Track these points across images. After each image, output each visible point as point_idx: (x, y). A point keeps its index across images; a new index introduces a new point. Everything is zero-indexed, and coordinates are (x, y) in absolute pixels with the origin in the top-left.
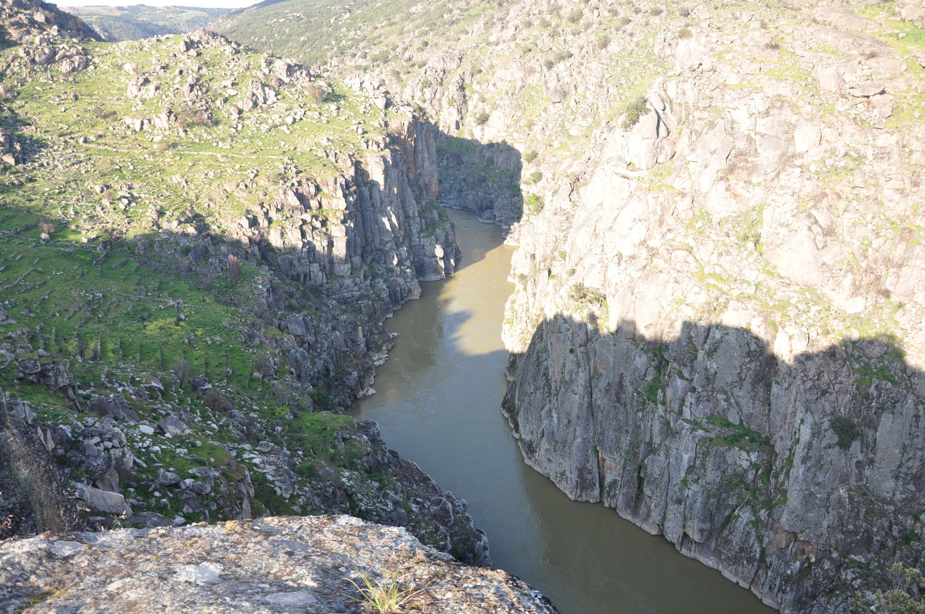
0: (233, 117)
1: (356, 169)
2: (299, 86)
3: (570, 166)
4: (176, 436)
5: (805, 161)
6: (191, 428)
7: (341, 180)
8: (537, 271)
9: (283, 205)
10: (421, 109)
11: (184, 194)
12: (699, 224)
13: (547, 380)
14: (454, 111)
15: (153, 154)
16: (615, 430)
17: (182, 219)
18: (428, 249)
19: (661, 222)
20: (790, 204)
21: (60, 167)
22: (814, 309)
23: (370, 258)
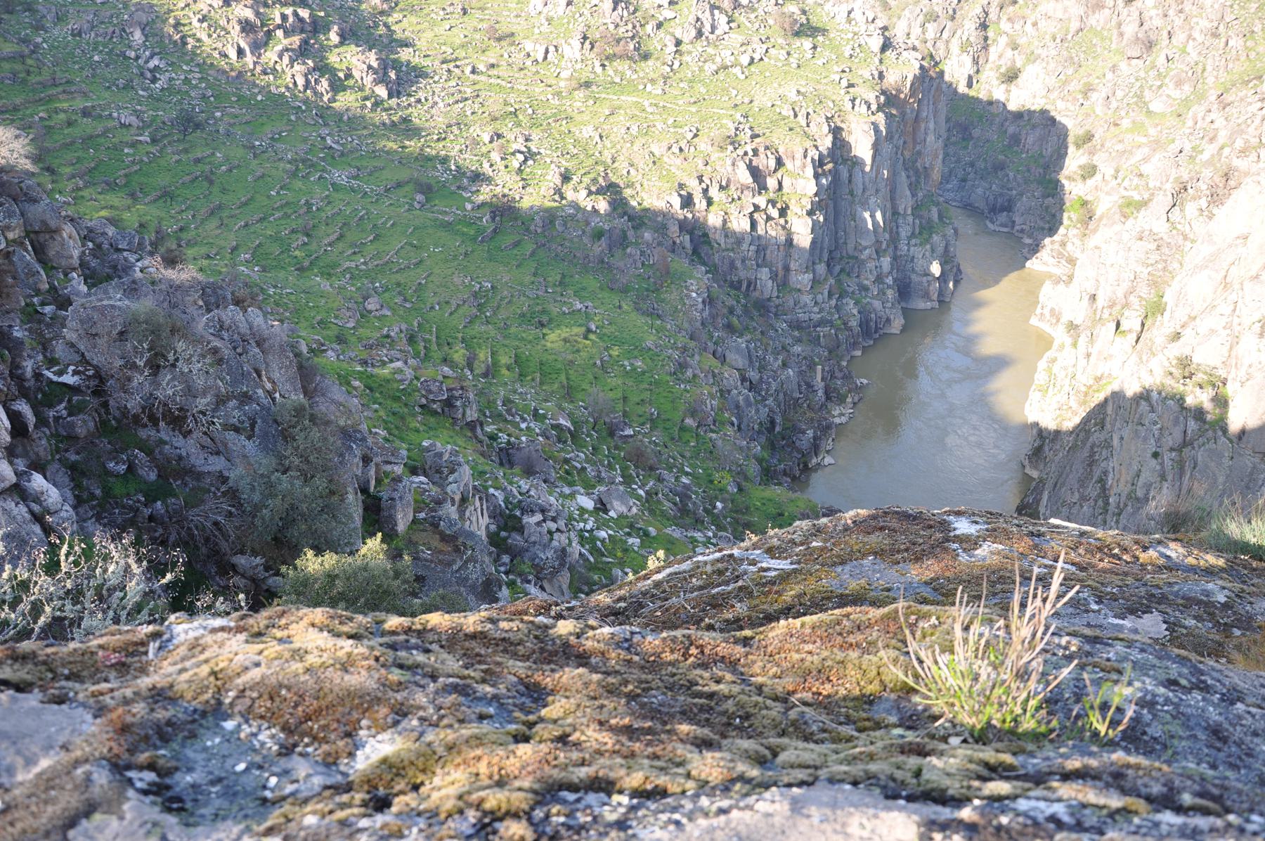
1: (835, 138)
4: (621, 516)
9: (729, 181)
11: (597, 154)
13: (1104, 489)
14: (967, 60)
15: (558, 94)
17: (593, 189)
18: (919, 264)
21: (441, 105)
23: (838, 268)
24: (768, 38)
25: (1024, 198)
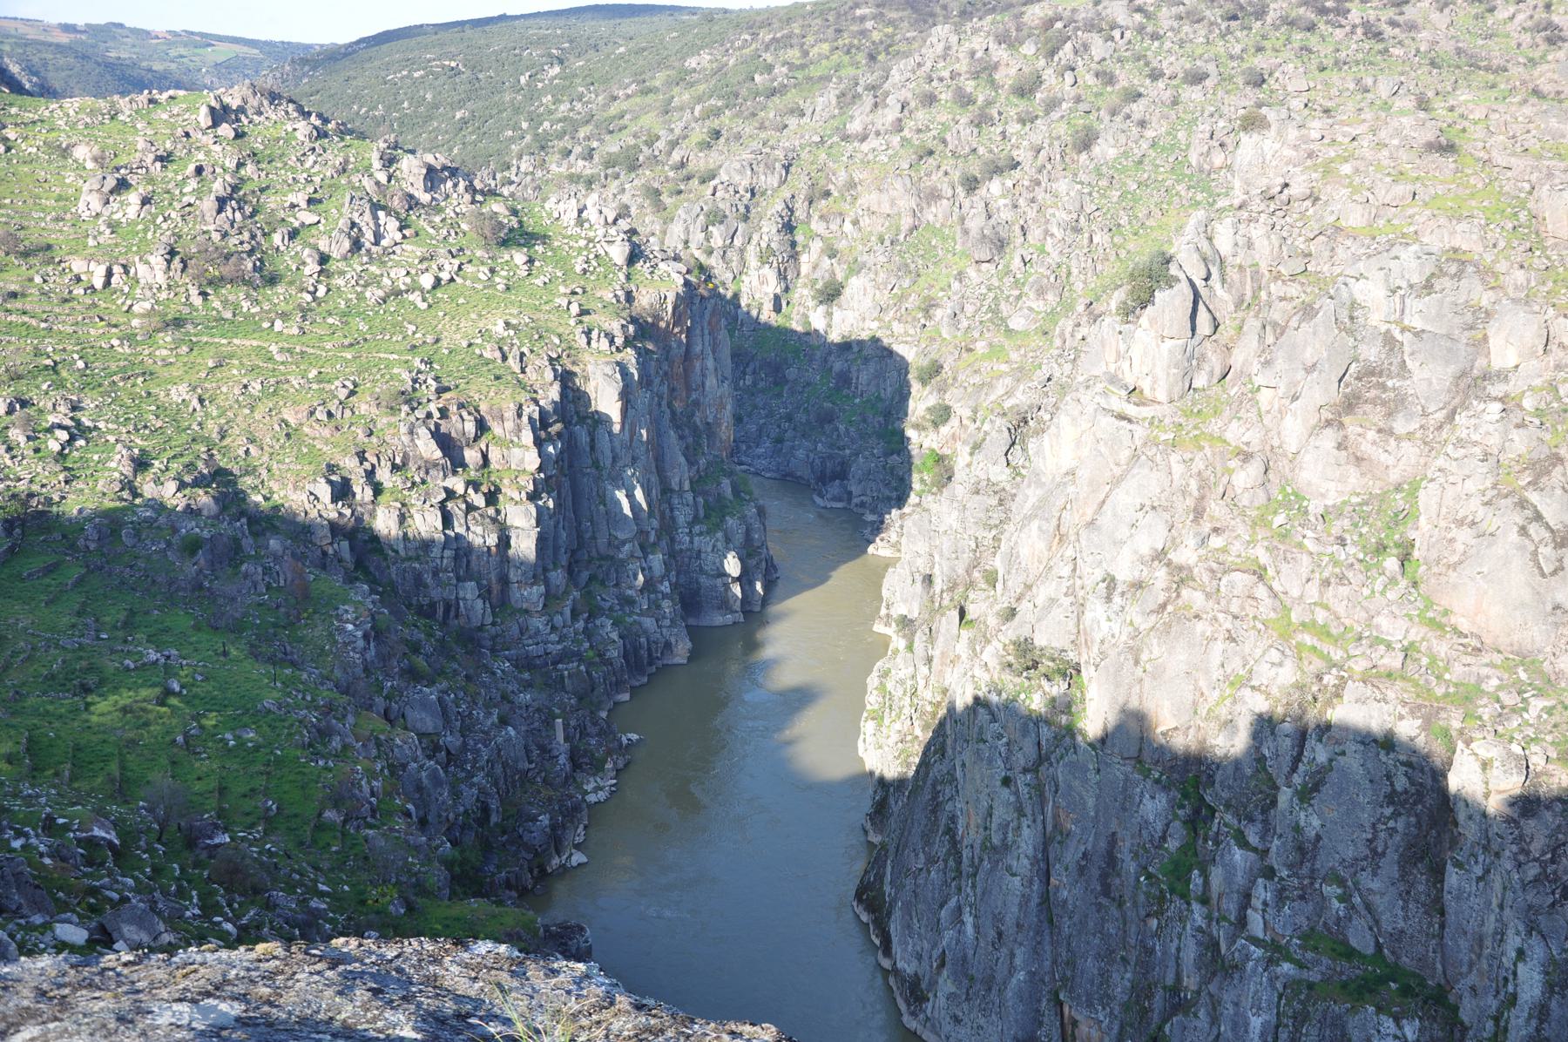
0: (307, 271)
2: (449, 212)
3: (1009, 394)
5: (1513, 387)
6: (174, 930)
7: (531, 410)
8: (934, 610)
10: (702, 268)
12: (1280, 519)
13: (954, 843)
14: (770, 274)
15: (129, 338)
16: (1098, 957)
17: (188, 479)
19: (1198, 513)
20: (1479, 480)
22: (1537, 705)
23: (585, 575)
24: (461, 250)
25: (861, 460)
